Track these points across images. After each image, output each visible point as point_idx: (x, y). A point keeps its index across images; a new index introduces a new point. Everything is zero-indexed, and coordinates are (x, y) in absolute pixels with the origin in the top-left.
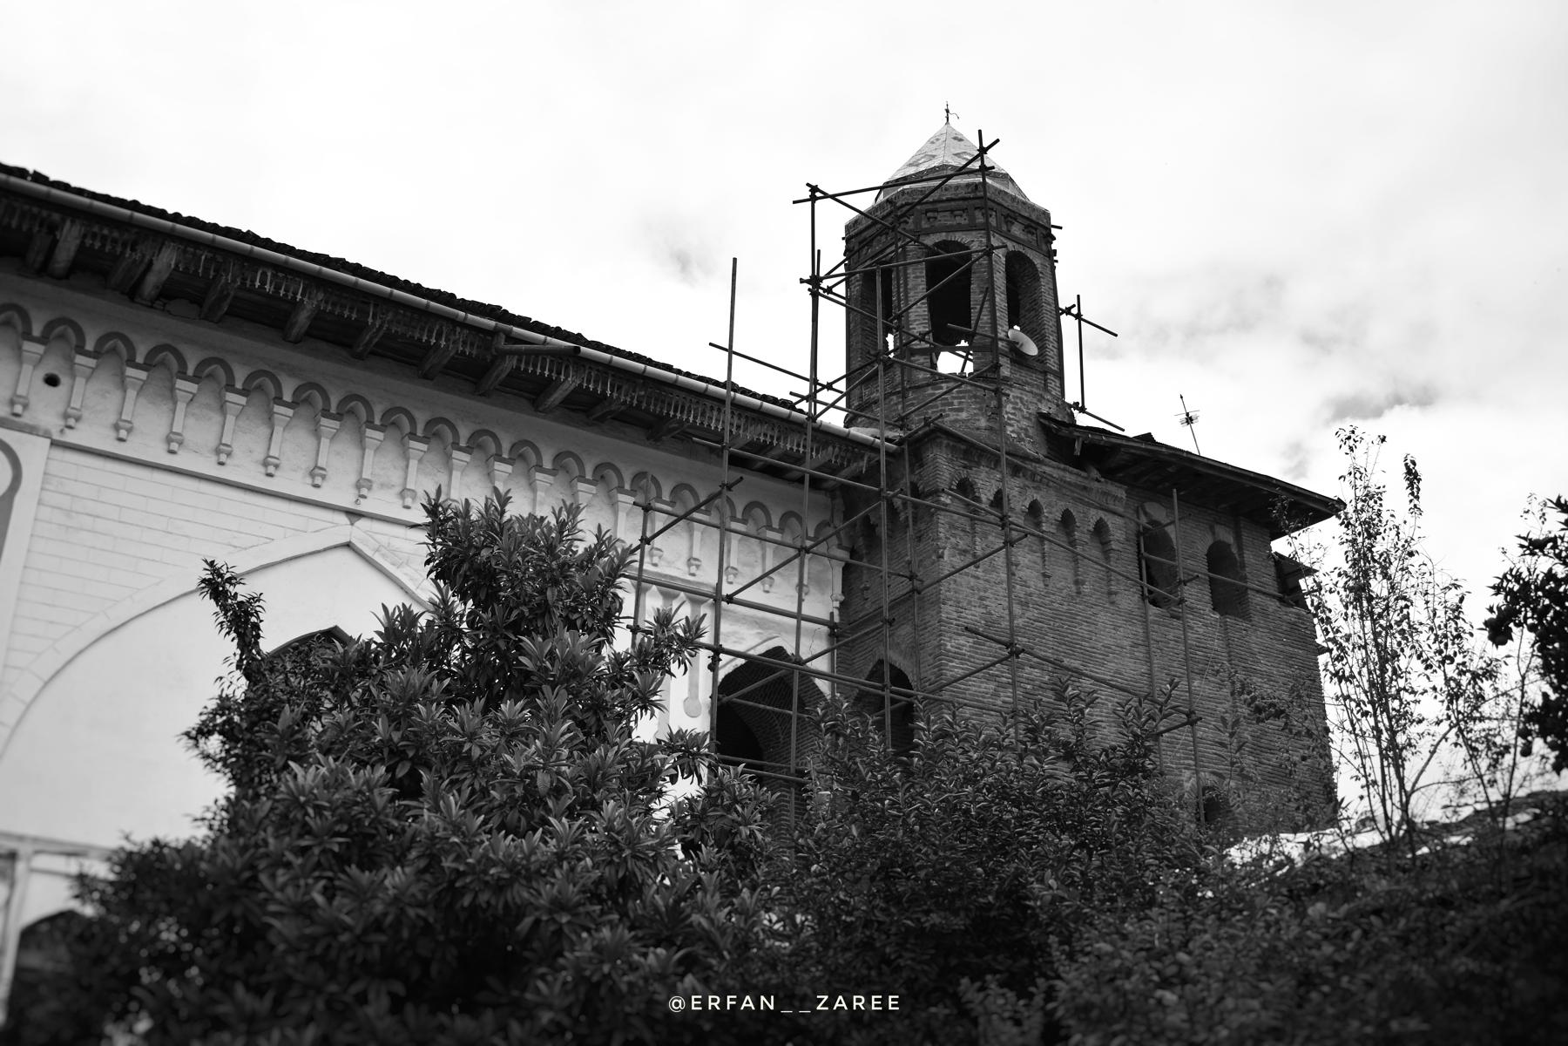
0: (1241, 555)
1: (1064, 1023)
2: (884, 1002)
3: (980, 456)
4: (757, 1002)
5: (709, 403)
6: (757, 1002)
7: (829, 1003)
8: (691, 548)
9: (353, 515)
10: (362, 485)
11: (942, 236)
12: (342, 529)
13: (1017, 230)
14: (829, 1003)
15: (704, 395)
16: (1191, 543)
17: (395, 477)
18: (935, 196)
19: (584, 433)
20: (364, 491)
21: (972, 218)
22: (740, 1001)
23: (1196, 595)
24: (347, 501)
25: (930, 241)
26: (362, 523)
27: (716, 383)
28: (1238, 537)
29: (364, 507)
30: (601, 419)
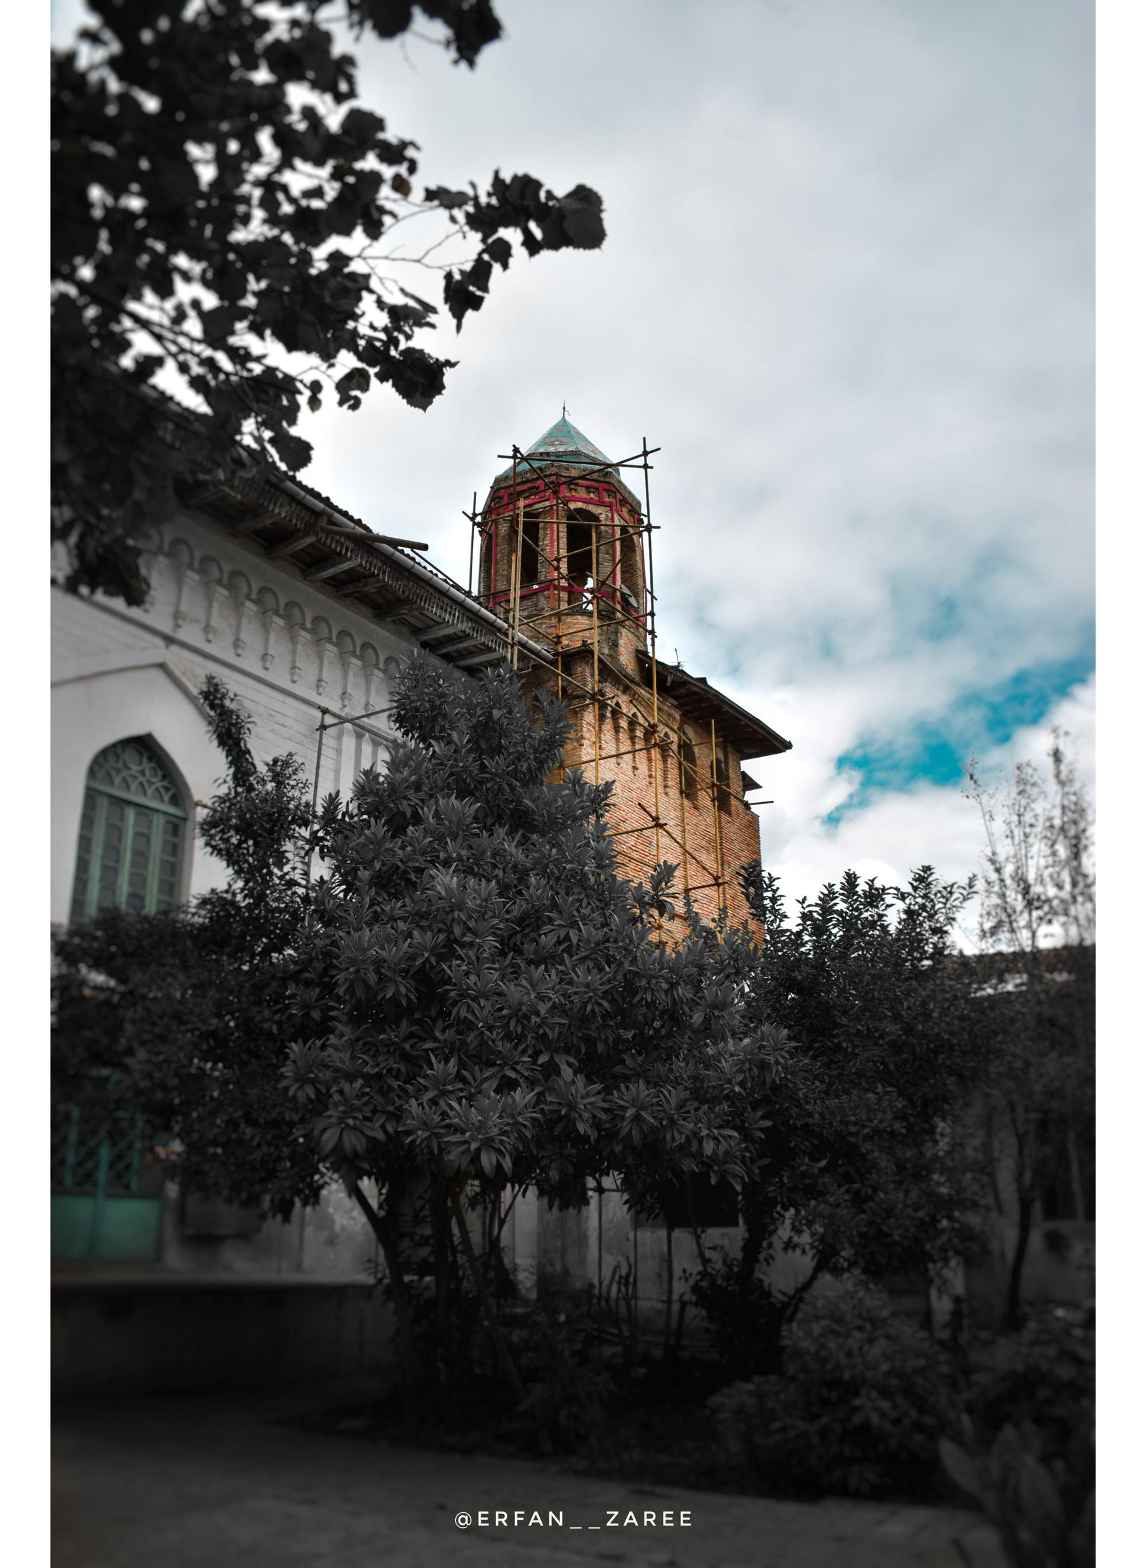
0: (727, 770)
1: (287, 855)
2: (676, 1518)
3: (608, 675)
4: (545, 1518)
5: (446, 600)
6: (545, 1518)
7: (620, 1519)
8: (321, 671)
9: (169, 640)
10: (177, 615)
11: (580, 505)
12: (159, 652)
13: (625, 511)
14: (620, 1519)
15: (444, 594)
16: (706, 756)
17: (201, 614)
18: (595, 476)
19: (335, 605)
20: (180, 622)
21: (600, 496)
22: (528, 1517)
23: (705, 798)
24: (166, 626)
25: (573, 506)
26: (174, 649)
27: (458, 588)
28: (726, 757)
29: (181, 635)
30: (346, 596)
